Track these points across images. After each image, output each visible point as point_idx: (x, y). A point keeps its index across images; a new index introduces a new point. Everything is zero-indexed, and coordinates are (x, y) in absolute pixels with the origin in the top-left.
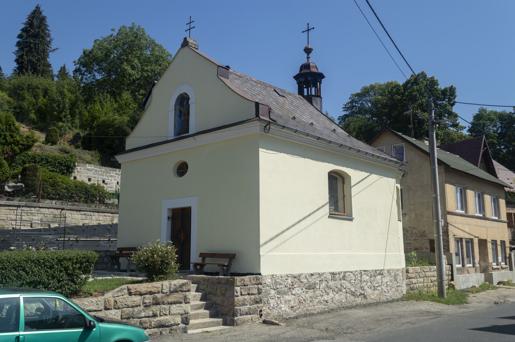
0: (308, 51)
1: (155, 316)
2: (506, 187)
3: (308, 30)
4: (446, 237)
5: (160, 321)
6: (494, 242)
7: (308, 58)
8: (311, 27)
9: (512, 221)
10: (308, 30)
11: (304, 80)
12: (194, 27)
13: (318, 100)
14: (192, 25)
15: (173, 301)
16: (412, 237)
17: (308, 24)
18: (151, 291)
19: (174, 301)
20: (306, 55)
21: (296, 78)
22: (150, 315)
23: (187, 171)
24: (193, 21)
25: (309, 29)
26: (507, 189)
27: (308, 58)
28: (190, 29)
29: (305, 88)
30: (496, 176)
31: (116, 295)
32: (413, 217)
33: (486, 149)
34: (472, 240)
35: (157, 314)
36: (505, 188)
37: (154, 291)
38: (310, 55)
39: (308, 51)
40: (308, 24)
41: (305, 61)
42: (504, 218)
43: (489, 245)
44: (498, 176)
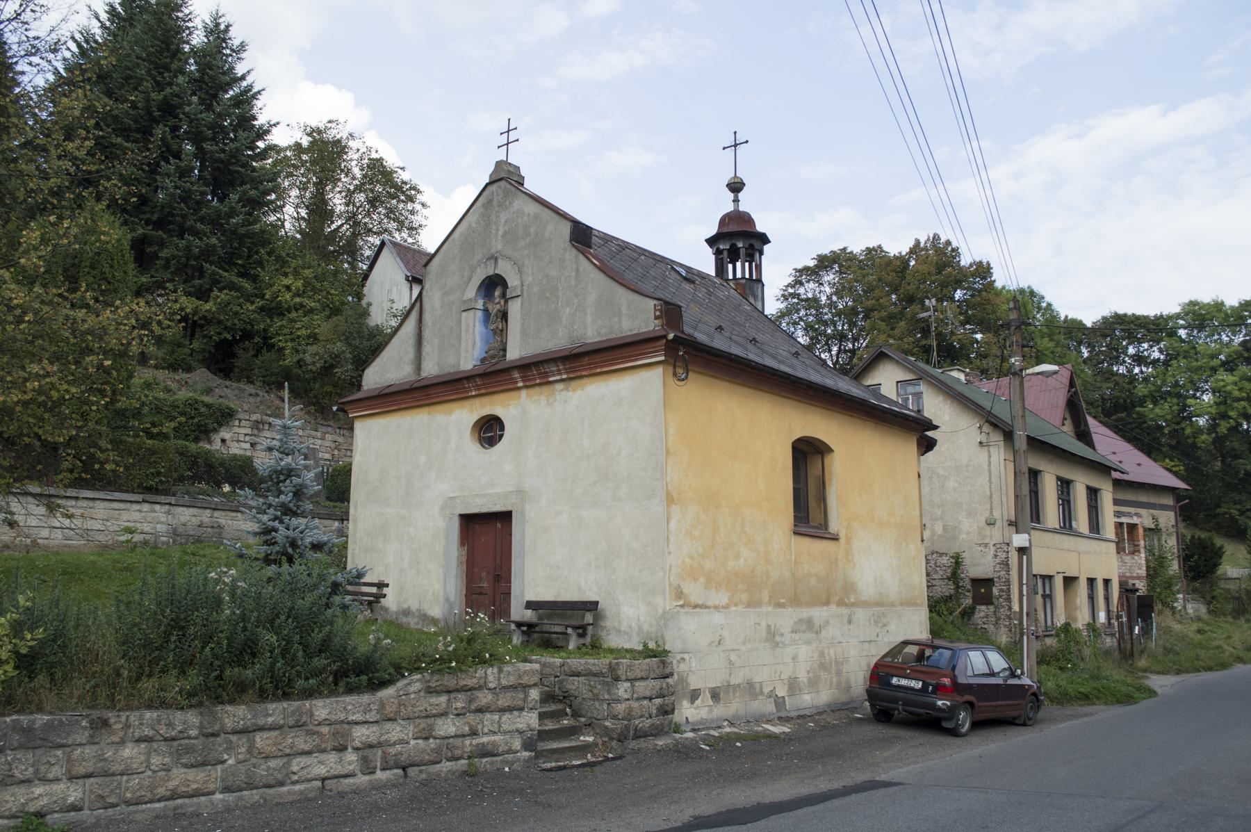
0: (736, 187)
1: (474, 733)
2: (1115, 470)
3: (736, 145)
4: (1004, 573)
5: (483, 744)
6: (1091, 581)
7: (736, 201)
8: (740, 139)
9: (1124, 539)
10: (736, 145)
11: (728, 247)
12: (499, 147)
13: (758, 288)
14: (513, 136)
15: (507, 704)
16: (936, 572)
17: (735, 133)
18: (467, 685)
19: (509, 706)
20: (731, 196)
21: (711, 241)
22: (465, 733)
23: (501, 436)
24: (501, 134)
25: (737, 142)
26: (1115, 475)
27: (736, 201)
28: (507, 144)
29: (730, 262)
30: (1093, 448)
31: (401, 693)
32: (939, 533)
33: (1075, 393)
34: (1050, 577)
35: (477, 731)
36: (1113, 472)
37: (472, 685)
38: (741, 195)
39: (736, 187)
40: (735, 133)
41: (730, 207)
42: (1109, 531)
43: (1100, 586)
44: (1097, 448)
